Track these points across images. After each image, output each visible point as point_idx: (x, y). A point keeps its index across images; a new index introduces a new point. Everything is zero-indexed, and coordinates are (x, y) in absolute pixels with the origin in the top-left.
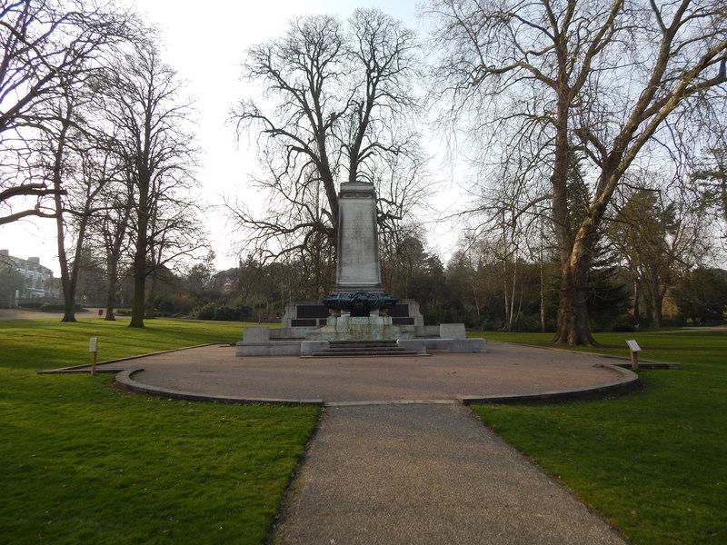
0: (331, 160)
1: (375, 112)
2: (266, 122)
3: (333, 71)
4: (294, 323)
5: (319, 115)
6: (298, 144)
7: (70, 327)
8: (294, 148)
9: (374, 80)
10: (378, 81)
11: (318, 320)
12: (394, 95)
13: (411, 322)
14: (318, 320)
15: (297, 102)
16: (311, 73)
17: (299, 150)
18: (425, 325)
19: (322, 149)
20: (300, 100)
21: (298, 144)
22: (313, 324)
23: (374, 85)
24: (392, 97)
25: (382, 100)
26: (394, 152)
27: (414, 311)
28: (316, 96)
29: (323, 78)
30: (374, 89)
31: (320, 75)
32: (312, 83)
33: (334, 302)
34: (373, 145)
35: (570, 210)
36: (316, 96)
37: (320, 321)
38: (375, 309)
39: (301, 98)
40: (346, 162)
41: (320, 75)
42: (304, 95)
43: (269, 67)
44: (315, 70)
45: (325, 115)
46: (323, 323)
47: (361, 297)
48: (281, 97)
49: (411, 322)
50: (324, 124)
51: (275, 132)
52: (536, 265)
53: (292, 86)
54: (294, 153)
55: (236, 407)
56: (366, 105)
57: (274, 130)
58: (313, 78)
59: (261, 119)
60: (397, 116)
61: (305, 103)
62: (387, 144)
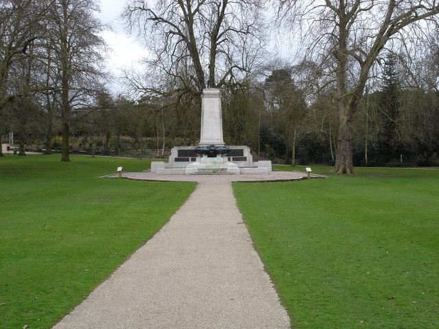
0: (198, 44)
4: (177, 160)
6: (172, 28)
7: (21, 160)
8: (171, 32)
11: (190, 158)
13: (245, 159)
14: (190, 158)
18: (253, 161)
19: (191, 33)
22: (187, 160)
26: (244, 33)
27: (247, 152)
33: (200, 150)
40: (208, 43)
46: (194, 160)
49: (245, 159)
52: (144, 99)
55: (166, 183)
56: (222, 5)
57: (156, 18)
62: (237, 27)
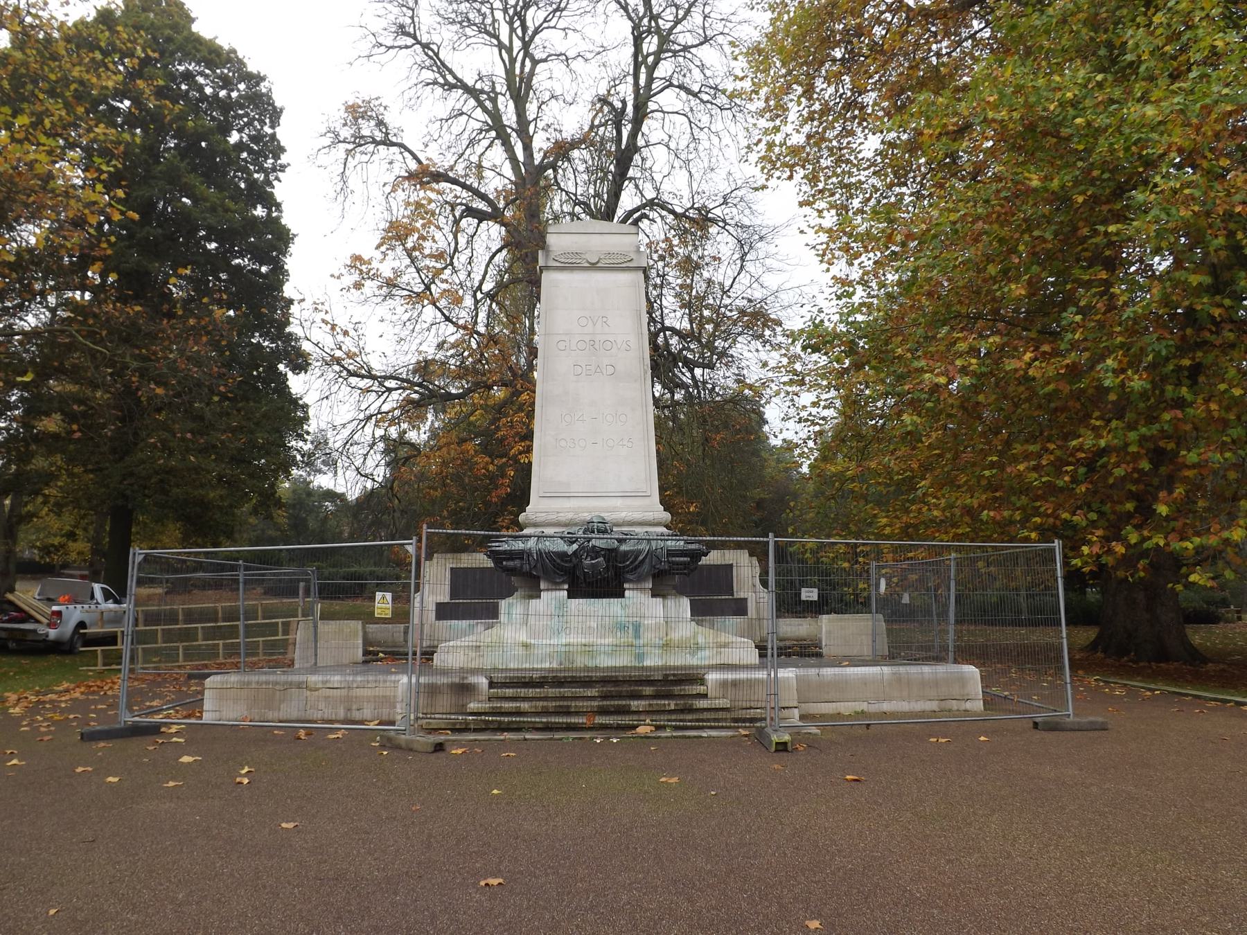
1: (652, 128)
2: (406, 154)
3: (560, 49)
5: (527, 148)
8: (470, 212)
9: (651, 59)
10: (656, 63)
12: (696, 88)
13: (740, 608)
15: (479, 113)
16: (510, 50)
17: (481, 216)
20: (485, 110)
21: (481, 205)
23: (651, 69)
24: (689, 91)
25: (668, 99)
28: (520, 101)
29: (535, 62)
30: (650, 80)
31: (527, 54)
32: (509, 72)
34: (651, 204)
35: (257, 371)
36: (520, 101)
37: (185, 648)
38: (640, 579)
39: (488, 104)
41: (527, 54)
42: (494, 101)
43: (414, 37)
44: (517, 44)
45: (541, 142)
47: (599, 542)
48: (439, 103)
49: (740, 608)
50: (538, 158)
51: (425, 176)
53: (470, 83)
54: (468, 223)
58: (513, 61)
59: (395, 149)
60: (702, 136)
61: (495, 115)
